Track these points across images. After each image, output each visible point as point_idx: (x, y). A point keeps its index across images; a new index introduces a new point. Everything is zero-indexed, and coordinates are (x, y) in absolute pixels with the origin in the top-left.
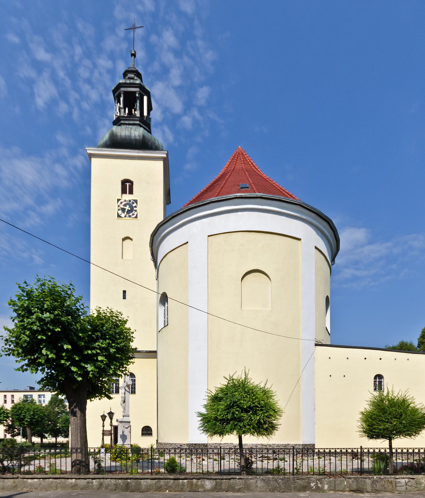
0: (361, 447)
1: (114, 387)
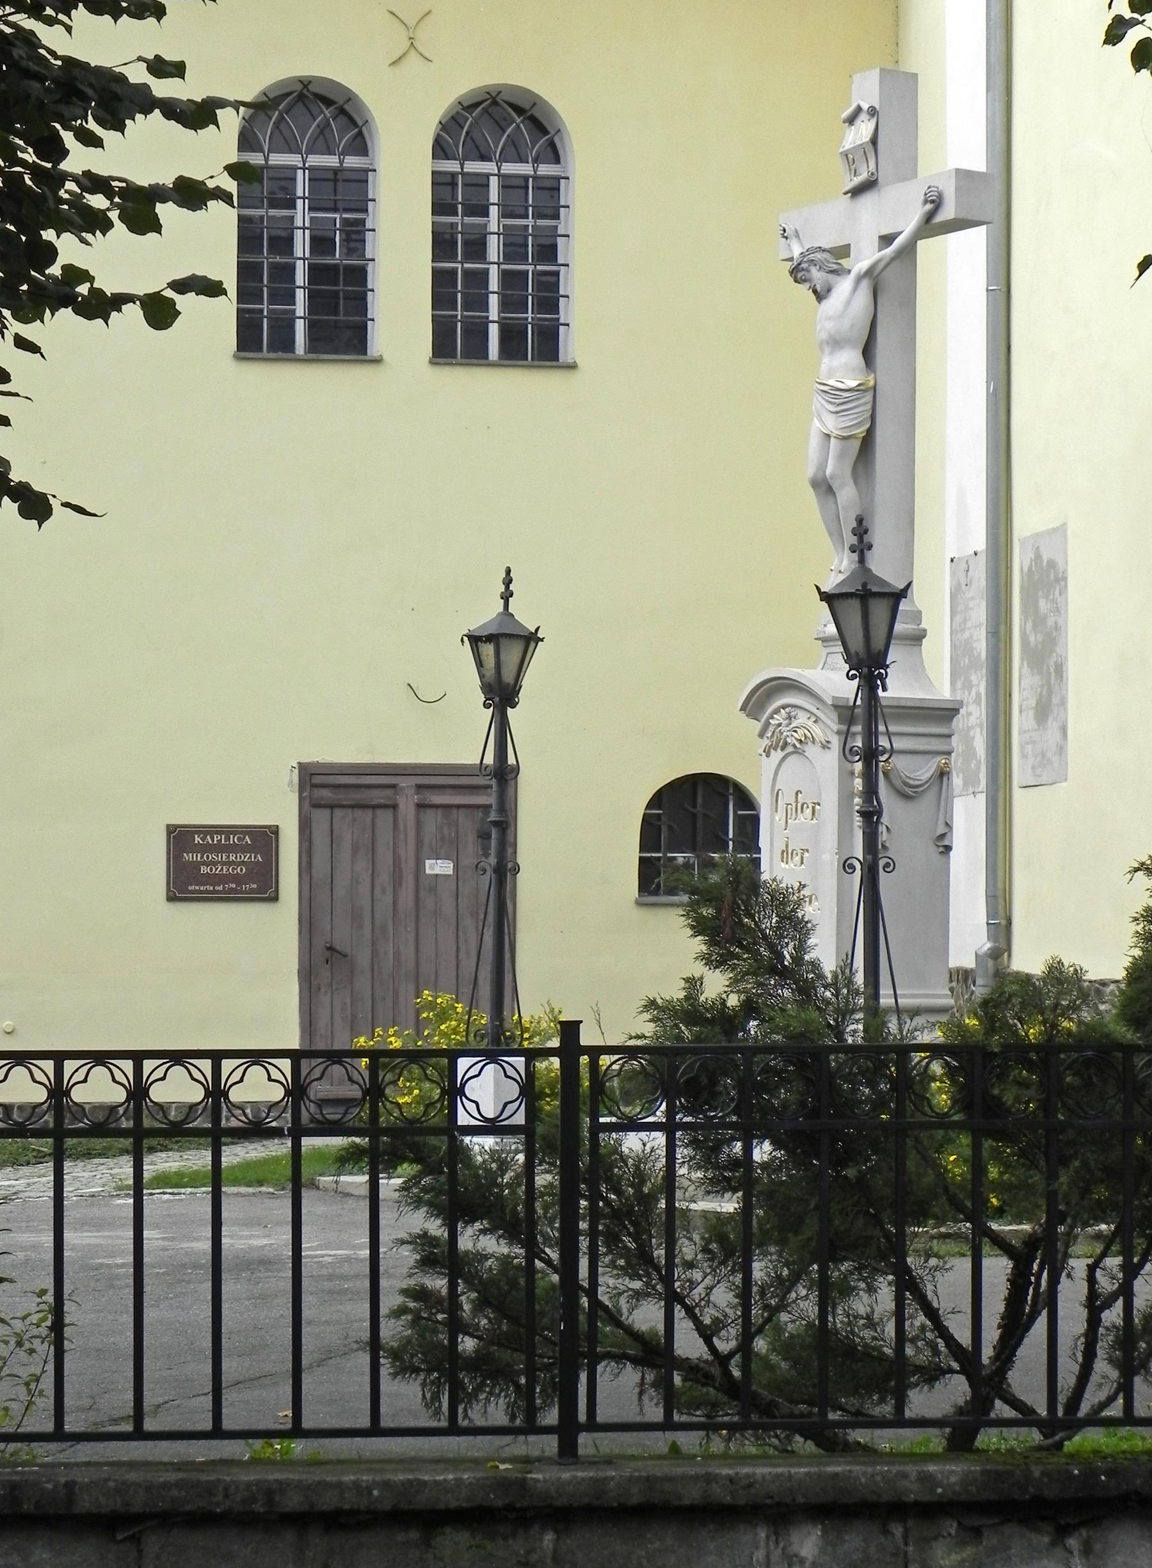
0: (570, 1030)
1: (300, 277)
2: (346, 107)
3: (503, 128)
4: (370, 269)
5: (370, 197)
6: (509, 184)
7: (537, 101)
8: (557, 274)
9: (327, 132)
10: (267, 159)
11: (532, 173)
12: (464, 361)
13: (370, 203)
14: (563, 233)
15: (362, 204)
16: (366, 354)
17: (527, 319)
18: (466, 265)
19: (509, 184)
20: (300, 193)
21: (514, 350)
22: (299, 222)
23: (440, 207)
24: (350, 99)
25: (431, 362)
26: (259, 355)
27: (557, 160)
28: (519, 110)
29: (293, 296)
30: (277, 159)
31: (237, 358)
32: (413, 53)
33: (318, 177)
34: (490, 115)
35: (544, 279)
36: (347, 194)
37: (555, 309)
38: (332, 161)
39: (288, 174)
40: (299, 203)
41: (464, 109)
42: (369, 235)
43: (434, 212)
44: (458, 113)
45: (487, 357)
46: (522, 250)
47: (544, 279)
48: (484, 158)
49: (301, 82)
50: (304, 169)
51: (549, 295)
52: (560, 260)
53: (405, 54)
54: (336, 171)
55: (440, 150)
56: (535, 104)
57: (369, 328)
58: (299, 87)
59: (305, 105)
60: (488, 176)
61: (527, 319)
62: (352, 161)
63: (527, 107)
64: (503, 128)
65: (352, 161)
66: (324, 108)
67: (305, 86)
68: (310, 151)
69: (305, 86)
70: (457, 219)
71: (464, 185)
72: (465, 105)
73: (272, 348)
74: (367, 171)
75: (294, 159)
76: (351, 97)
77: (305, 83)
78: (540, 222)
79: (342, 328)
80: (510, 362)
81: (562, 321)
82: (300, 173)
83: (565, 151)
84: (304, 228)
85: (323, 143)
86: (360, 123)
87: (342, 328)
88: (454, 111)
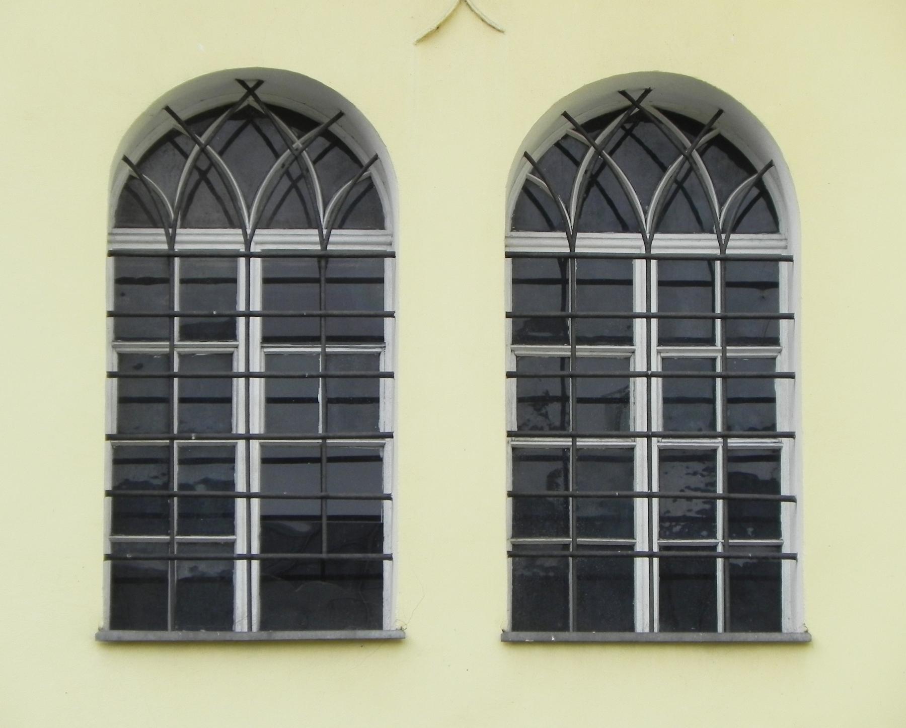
2: (335, 128)
3: (659, 167)
4: (387, 455)
5: (783, 310)
6: (678, 277)
7: (723, 107)
8: (774, 456)
9: (212, 176)
10: (324, 241)
11: (717, 252)
12: (264, 635)
13: (783, 323)
14: (785, 370)
15: (370, 326)
16: (380, 626)
17: (714, 548)
18: (733, 442)
19: (678, 277)
20: (639, 306)
21: (687, 613)
22: (639, 364)
23: (126, 320)
24: (341, 114)
25: (506, 639)
26: (563, 635)
27: (772, 224)
28: (691, 126)
29: (230, 515)
30: (592, 243)
31: (105, 640)
32: (464, 13)
33: (281, 273)
34: (634, 137)
35: (745, 468)
36: (339, 310)
37: (772, 526)
38: (305, 240)
39: (219, 268)
40: (639, 325)
41: (577, 128)
42: (780, 386)
43: (519, 337)
44: (566, 137)
45: (631, 627)
46: (705, 407)
47: (745, 468)
48: (626, 225)
49: (242, 83)
50: (648, 258)
51: (758, 500)
52: (781, 427)
53: (447, 20)
54: (562, 260)
55: (533, 206)
56: (720, 112)
57: (386, 575)
58: (238, 93)
59: (258, 130)
60: (630, 258)
61: (714, 548)
62: (346, 240)
63: (705, 119)
64: (659, 167)
65: (346, 240)
66: (291, 133)
67: (251, 92)
68: (660, 226)
69: (251, 92)
70: (714, 351)
71: (728, 285)
72: (580, 120)
73: (737, 622)
74: (776, 260)
75: (227, 239)
76: (342, 112)
77: (250, 83)
78: (734, 351)
79: (331, 579)
80: (191, 635)
81: (786, 550)
82: (639, 266)
83: (785, 205)
84: (248, 375)
85: (683, 208)
86: (760, 167)
87: (331, 579)
88: (558, 135)
